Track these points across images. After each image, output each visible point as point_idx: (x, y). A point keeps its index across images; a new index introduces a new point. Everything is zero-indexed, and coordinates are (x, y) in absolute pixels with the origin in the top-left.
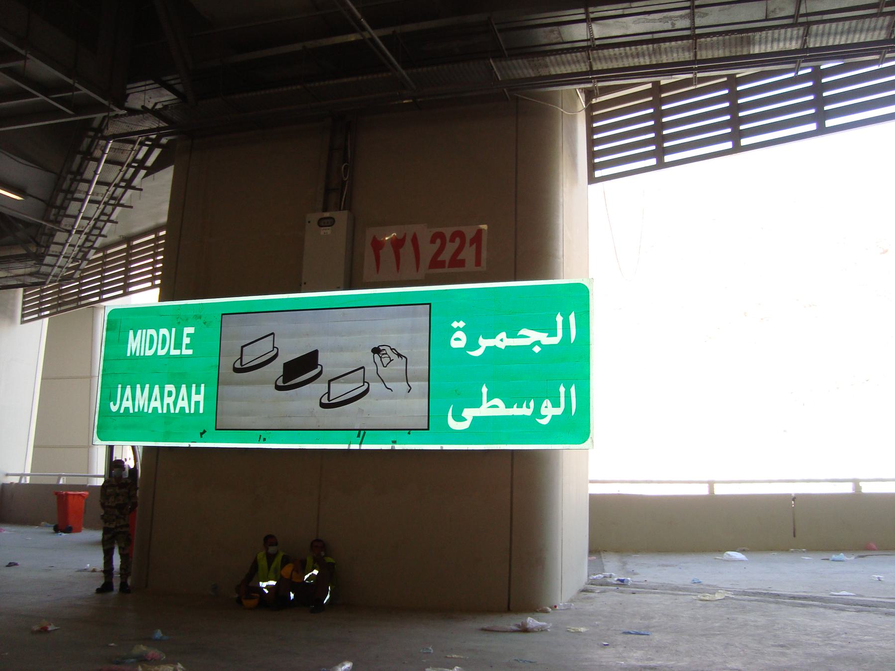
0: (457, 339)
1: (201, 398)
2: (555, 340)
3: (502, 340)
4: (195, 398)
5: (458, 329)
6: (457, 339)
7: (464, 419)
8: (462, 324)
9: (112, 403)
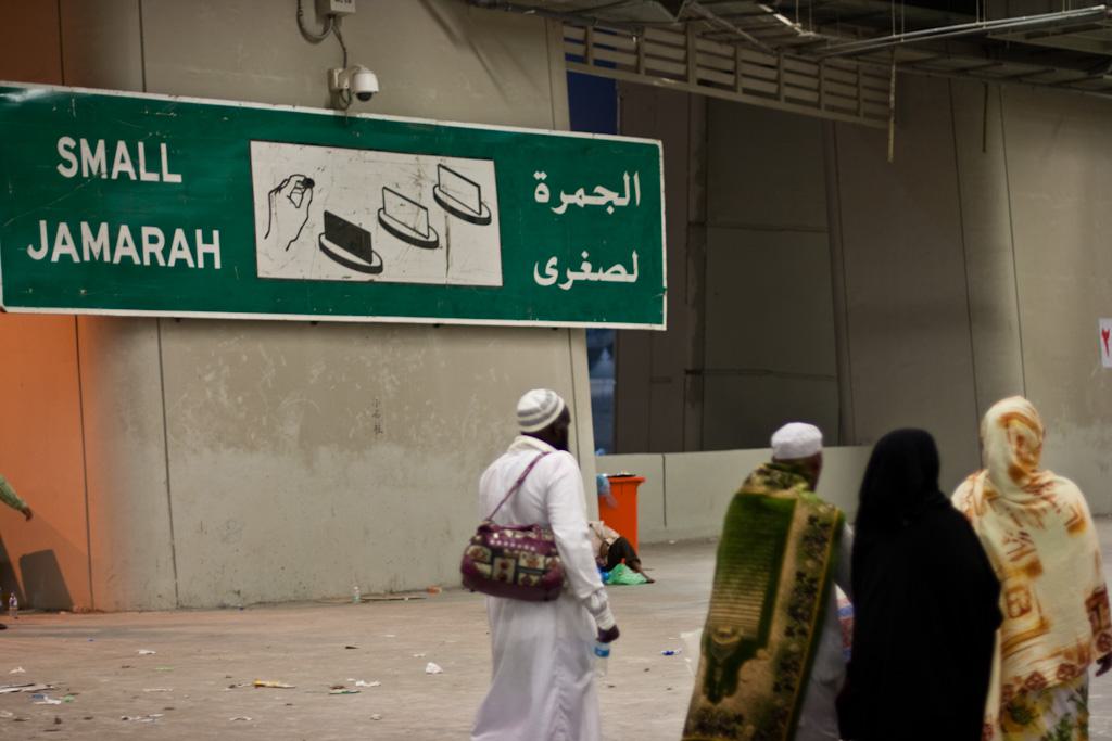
0: (541, 193)
1: (215, 249)
2: (624, 202)
3: (580, 197)
4: (202, 248)
5: (540, 181)
6: (541, 193)
7: (549, 276)
8: (543, 176)
9: (61, 169)
